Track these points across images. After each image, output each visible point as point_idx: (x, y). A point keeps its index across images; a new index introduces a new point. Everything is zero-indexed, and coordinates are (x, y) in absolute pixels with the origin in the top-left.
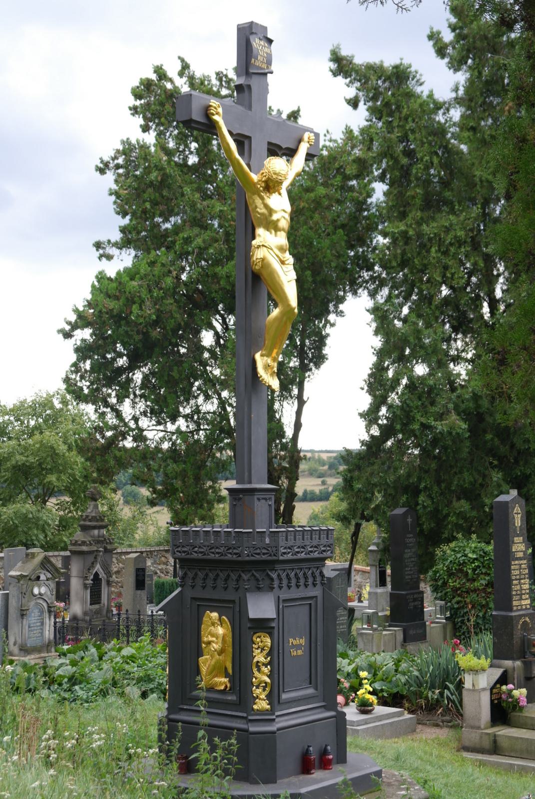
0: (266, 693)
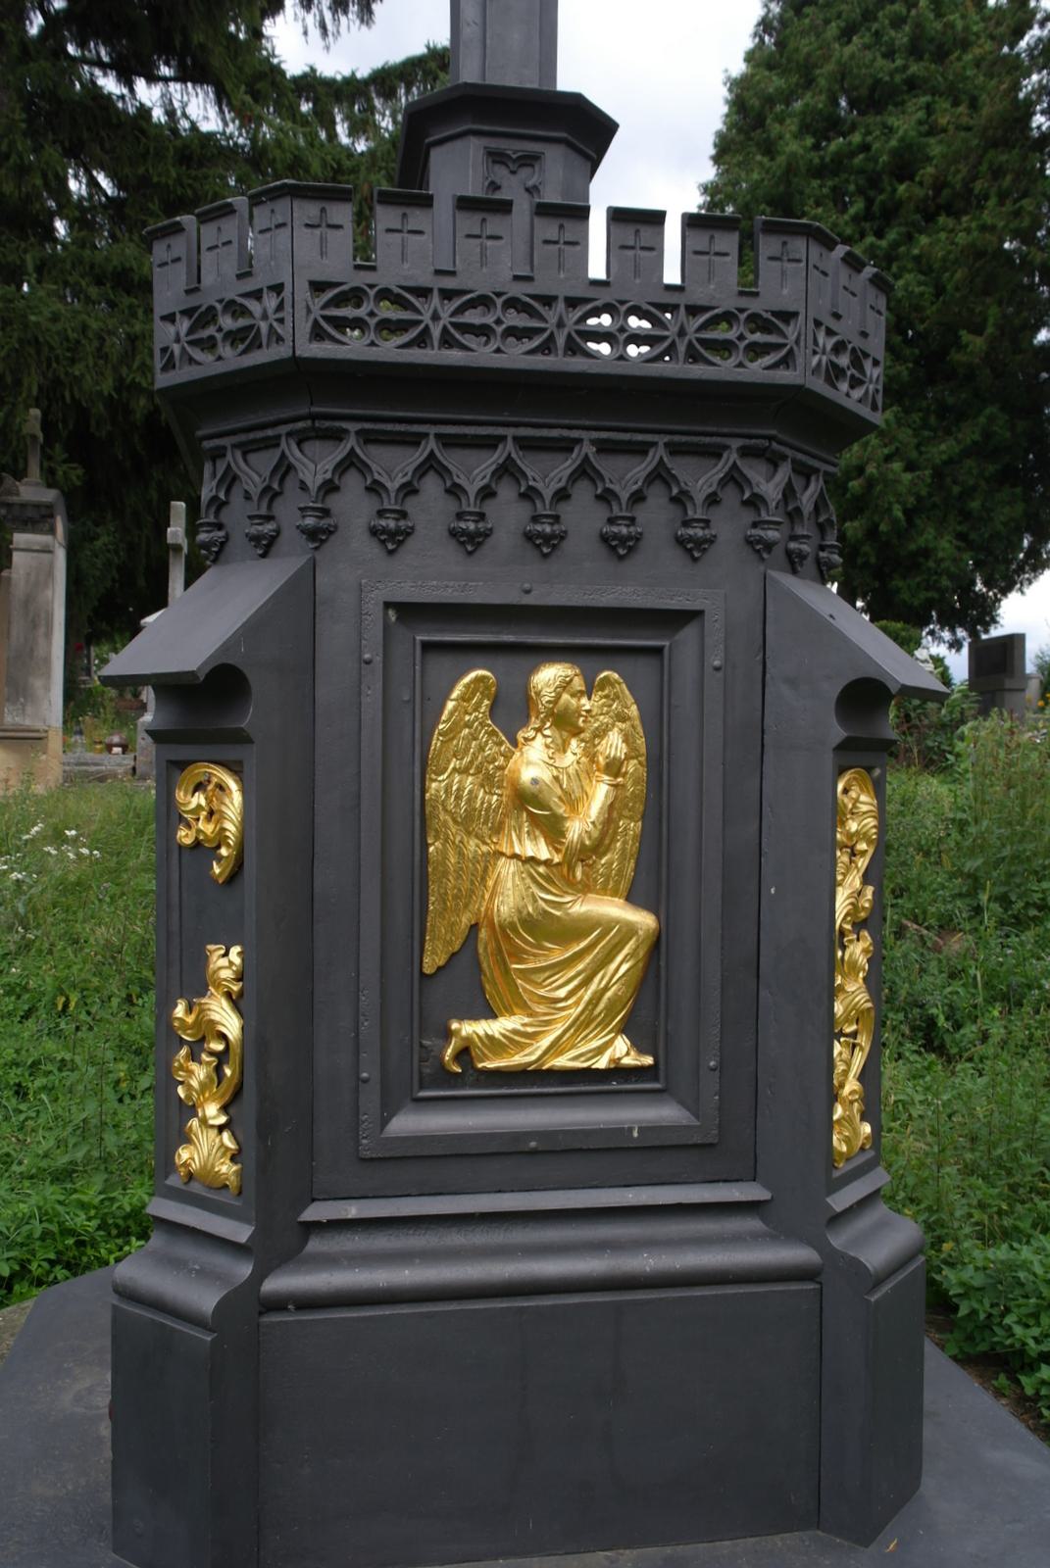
0: (227, 1088)
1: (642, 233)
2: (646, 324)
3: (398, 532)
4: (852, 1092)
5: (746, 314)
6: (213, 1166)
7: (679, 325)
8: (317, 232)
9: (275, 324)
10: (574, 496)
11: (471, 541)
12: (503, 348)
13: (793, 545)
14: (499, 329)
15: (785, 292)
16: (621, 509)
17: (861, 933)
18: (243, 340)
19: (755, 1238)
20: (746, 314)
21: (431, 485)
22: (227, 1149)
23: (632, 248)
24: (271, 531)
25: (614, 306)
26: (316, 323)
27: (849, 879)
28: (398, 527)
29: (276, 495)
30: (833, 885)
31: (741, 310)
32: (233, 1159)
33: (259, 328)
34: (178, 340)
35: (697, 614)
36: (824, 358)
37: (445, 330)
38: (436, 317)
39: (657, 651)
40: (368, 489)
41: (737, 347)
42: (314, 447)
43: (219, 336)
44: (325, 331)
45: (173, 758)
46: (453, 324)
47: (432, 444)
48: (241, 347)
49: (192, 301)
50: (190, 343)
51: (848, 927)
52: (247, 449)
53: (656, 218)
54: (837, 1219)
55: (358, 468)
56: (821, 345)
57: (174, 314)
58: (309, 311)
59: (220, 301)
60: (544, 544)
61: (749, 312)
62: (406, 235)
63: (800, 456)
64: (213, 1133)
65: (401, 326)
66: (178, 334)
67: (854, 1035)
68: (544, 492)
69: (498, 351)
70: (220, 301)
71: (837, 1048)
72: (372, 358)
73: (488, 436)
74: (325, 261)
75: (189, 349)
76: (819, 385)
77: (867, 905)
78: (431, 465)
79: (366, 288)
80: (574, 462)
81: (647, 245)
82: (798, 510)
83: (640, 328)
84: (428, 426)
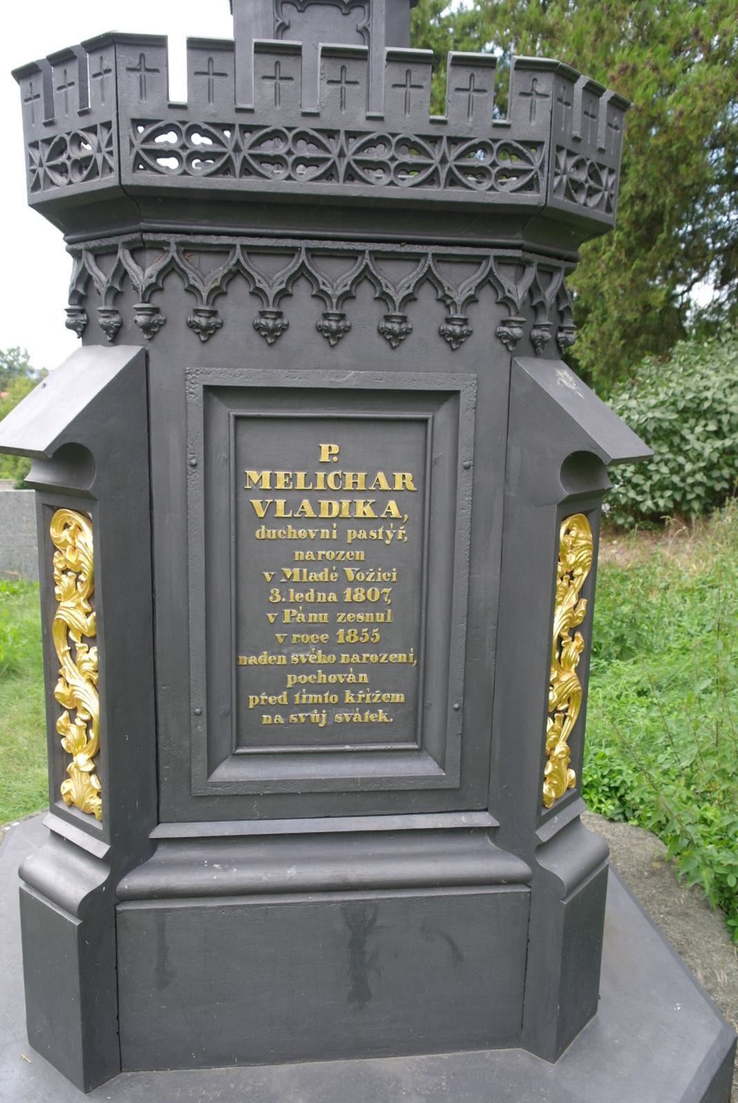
1: (413, 74)
2: (208, 141)
3: (275, 329)
4: (562, 753)
5: (498, 144)
6: (83, 800)
7: (441, 154)
8: (529, 99)
9: (107, 157)
10: (480, 301)
11: (272, 334)
12: (293, 176)
13: (536, 333)
14: (494, 171)
15: (533, 123)
16: (456, 312)
17: (576, 635)
18: (86, 167)
19: (488, 854)
20: (498, 144)
21: (427, 295)
22: (94, 789)
23: (404, 86)
25: (282, 132)
26: (138, 155)
27: (568, 597)
28: (401, 329)
30: (553, 605)
31: (495, 141)
32: (99, 794)
33: (95, 160)
35: (456, 393)
36: (565, 177)
37: (450, 171)
38: (237, 149)
39: (425, 421)
40: (251, 293)
41: (490, 173)
43: (69, 163)
44: (357, 173)
45: (48, 503)
46: (252, 155)
47: (367, 259)
49: (48, 133)
50: (51, 168)
51: (565, 634)
53: (159, 43)
54: (542, 847)
55: (370, 281)
56: (562, 167)
58: (132, 145)
59: (68, 134)
60: (272, 333)
61: (501, 142)
62: (212, 77)
63: (127, 238)
64: (84, 776)
65: (418, 168)
67: (566, 710)
68: (395, 298)
69: (492, 188)
70: (68, 134)
71: (550, 723)
72: (288, 191)
73: (286, 248)
74: (144, 102)
75: (49, 173)
76: (560, 201)
77: (581, 615)
78: (302, 273)
79: (285, 130)
80: (418, 274)
81: (417, 84)
82: (542, 304)
83: (203, 144)
84: (487, 249)
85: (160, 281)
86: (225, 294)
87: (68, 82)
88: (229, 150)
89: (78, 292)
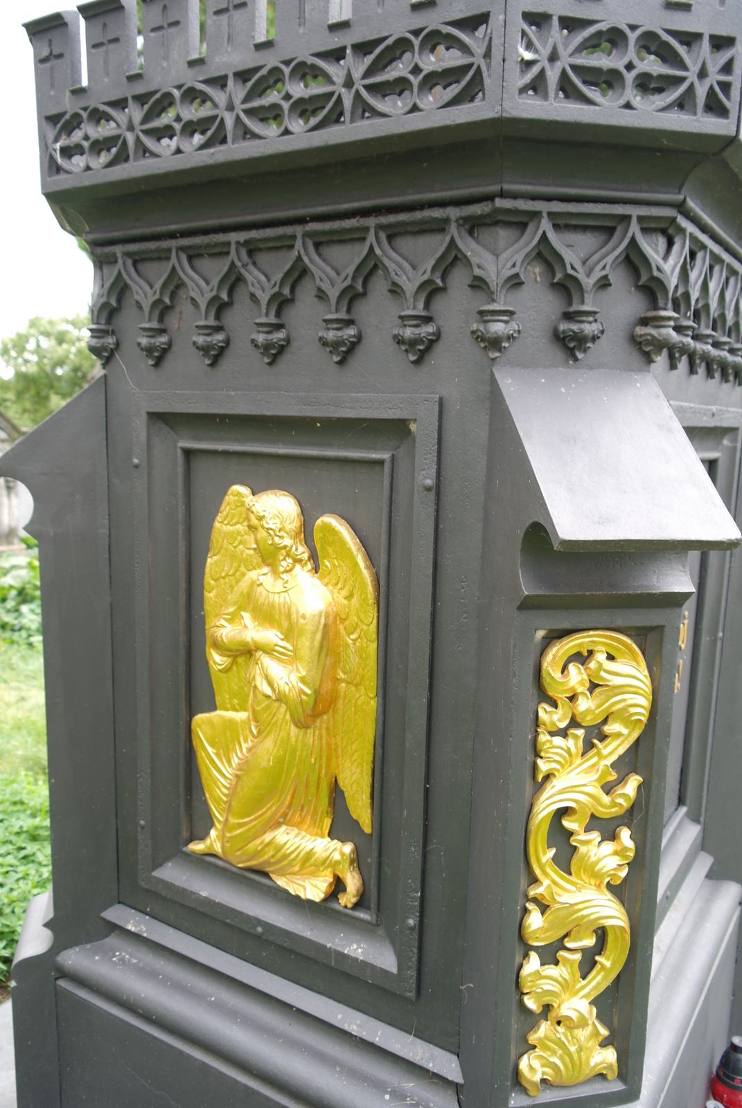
24: (429, 334)
29: (438, 290)
33: (222, 120)
34: (131, 128)
42: (407, 244)
47: (545, 225)
48: (314, 121)
50: (146, 132)
52: (193, 255)
57: (225, 77)
59: (179, 87)
66: (130, 121)
68: (329, 294)
70: (85, 109)
85: (439, 273)
86: (443, 289)
87: (103, 49)
88: (479, 60)
89: (164, 302)
